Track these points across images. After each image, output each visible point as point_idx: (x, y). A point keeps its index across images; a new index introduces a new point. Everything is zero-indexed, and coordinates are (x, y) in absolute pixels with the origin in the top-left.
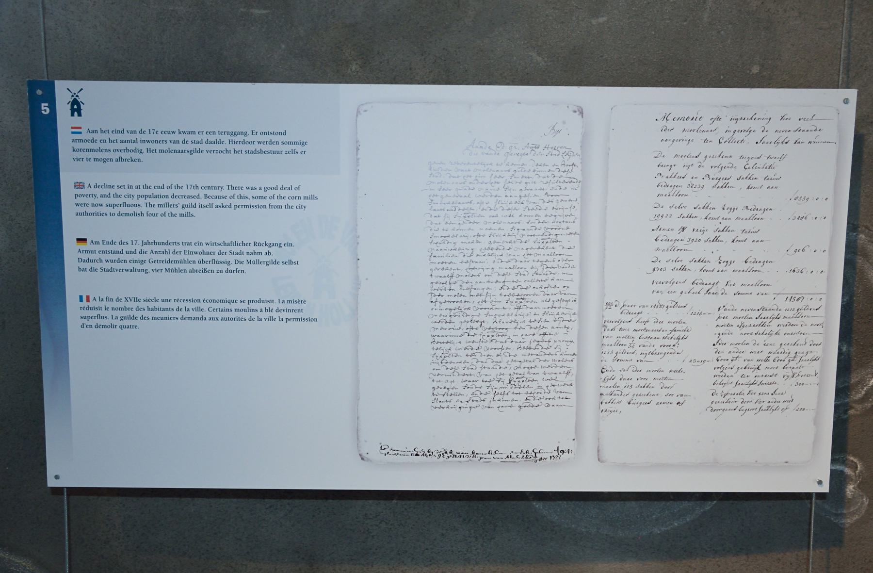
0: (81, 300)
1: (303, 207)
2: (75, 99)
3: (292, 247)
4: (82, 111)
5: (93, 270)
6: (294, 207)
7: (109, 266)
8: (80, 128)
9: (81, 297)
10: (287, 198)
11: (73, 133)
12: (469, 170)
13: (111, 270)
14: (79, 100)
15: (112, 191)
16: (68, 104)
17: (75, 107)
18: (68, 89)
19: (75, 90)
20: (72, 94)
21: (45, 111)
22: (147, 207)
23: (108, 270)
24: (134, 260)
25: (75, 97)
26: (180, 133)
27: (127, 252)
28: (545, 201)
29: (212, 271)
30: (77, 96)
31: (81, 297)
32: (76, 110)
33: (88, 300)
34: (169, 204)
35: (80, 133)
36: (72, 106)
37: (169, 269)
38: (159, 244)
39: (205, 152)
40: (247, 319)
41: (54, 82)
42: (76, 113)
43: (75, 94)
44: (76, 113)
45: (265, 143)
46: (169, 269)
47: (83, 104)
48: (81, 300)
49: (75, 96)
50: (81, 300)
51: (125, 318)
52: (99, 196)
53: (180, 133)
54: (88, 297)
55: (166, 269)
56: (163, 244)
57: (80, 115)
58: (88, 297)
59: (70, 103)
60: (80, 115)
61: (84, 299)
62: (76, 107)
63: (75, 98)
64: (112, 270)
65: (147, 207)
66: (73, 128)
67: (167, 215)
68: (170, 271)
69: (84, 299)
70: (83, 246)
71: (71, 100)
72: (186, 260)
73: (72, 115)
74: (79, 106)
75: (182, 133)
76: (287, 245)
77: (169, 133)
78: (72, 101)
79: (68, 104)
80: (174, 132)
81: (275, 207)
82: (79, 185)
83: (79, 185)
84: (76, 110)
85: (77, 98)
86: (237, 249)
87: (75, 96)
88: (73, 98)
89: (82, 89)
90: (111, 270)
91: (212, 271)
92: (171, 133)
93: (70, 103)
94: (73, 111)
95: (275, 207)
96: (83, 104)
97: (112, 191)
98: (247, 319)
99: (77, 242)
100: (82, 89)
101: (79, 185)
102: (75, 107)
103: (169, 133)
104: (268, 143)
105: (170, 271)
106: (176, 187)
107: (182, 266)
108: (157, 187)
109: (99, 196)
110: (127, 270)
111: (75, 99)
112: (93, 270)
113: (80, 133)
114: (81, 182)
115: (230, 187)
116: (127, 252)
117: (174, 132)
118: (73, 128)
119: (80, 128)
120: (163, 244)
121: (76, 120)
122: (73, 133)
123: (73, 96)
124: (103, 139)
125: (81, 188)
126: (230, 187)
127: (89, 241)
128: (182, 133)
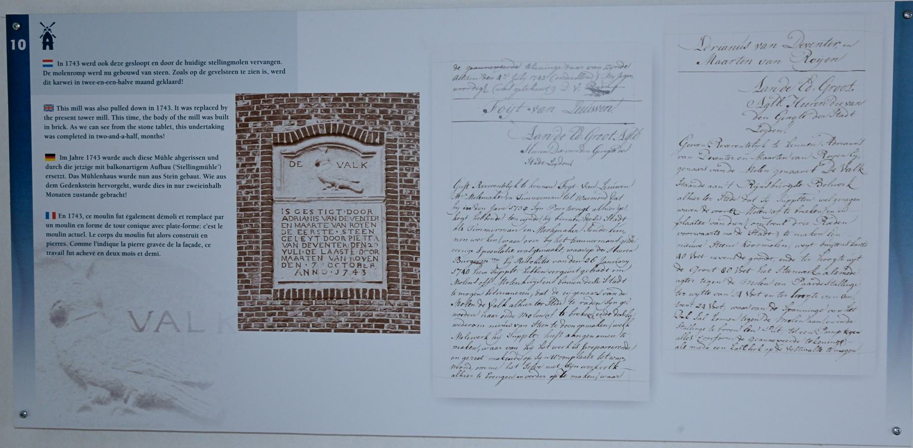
0: (47, 217)
2: (47, 33)
3: (108, 120)
8: (51, 61)
9: (47, 214)
11: (44, 66)
12: (517, 111)
14: (51, 34)
16: (41, 37)
17: (47, 40)
18: (41, 23)
20: (44, 28)
22: (58, 110)
24: (91, 135)
25: (47, 31)
27: (176, 177)
28: (583, 143)
30: (50, 30)
31: (47, 214)
32: (47, 43)
33: (54, 217)
34: (122, 107)
35: (51, 66)
37: (159, 156)
42: (48, 47)
43: (47, 28)
44: (48, 47)
46: (159, 156)
47: (55, 37)
48: (47, 217)
49: (47, 29)
51: (134, 245)
54: (54, 214)
55: (156, 156)
57: (51, 48)
58: (54, 214)
61: (51, 216)
65: (58, 110)
66: (44, 61)
67: (176, 117)
68: (160, 158)
69: (51, 216)
70: (51, 162)
71: (44, 34)
72: (211, 165)
73: (44, 48)
76: (90, 186)
79: (41, 37)
85: (49, 32)
88: (45, 32)
89: (54, 23)
96: (55, 37)
100: (54, 23)
101: (48, 108)
102: (47, 40)
105: (160, 158)
111: (47, 33)
113: (51, 66)
115: (60, 108)
116: (176, 177)
118: (44, 61)
119: (51, 61)
121: (48, 52)
122: (44, 66)
123: (45, 30)
127: (57, 157)
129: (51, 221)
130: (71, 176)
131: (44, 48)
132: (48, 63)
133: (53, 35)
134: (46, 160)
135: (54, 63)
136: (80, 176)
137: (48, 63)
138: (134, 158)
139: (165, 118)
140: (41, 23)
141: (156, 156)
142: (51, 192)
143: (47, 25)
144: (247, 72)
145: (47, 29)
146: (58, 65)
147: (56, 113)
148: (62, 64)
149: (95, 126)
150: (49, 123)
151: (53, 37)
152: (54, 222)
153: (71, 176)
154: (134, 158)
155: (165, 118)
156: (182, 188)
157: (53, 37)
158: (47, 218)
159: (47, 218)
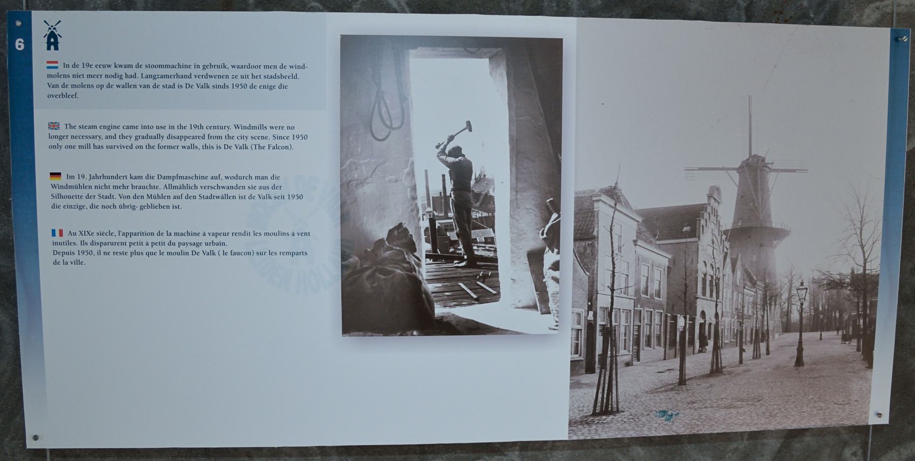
0: (54, 234)
1: (245, 137)
4: (59, 44)
5: (94, 207)
6: (236, 138)
7: (207, 193)
8: (56, 62)
9: (54, 231)
10: (121, 127)
11: (48, 67)
13: (210, 197)
14: (56, 33)
15: (118, 132)
16: (45, 37)
17: (52, 40)
19: (52, 23)
20: (49, 27)
21: (20, 42)
23: (207, 198)
25: (52, 30)
26: (116, 67)
29: (234, 197)
30: (55, 29)
31: (54, 231)
32: (52, 43)
35: (57, 67)
36: (49, 39)
37: (151, 195)
38: (108, 178)
39: (115, 87)
40: (89, 243)
41: (30, 13)
42: (52, 47)
43: (52, 26)
44: (52, 47)
45: (201, 77)
46: (151, 195)
47: (61, 37)
48: (54, 234)
50: (54, 234)
52: (103, 137)
53: (116, 67)
54: (61, 231)
55: (148, 195)
56: (112, 177)
57: (56, 48)
58: (61, 231)
59: (47, 36)
60: (56, 48)
61: (57, 233)
62: (53, 40)
63: (51, 31)
64: (211, 197)
66: (48, 62)
69: (57, 233)
70: (56, 181)
71: (48, 33)
73: (49, 49)
74: (56, 39)
75: (118, 66)
76: (66, 207)
77: (104, 66)
78: (49, 34)
79: (45, 37)
80: (109, 66)
81: (215, 138)
82: (54, 126)
83: (54, 126)
84: (52, 43)
85: (54, 31)
86: (102, 182)
87: (52, 28)
88: (50, 31)
89: (60, 22)
90: (210, 197)
91: (234, 197)
92: (106, 66)
93: (47, 36)
94: (49, 44)
95: (215, 138)
96: (61, 37)
97: (118, 132)
98: (89, 243)
99: (51, 177)
101: (54, 126)
102: (52, 40)
103: (104, 66)
104: (203, 77)
106: (179, 128)
107: (231, 192)
108: (212, 128)
109: (103, 137)
110: (218, 197)
112: (94, 207)
113: (57, 67)
114: (56, 123)
115: (68, 126)
117: (109, 66)
118: (48, 62)
119: (56, 62)
120: (112, 177)
121: (52, 54)
122: (48, 67)
123: (50, 29)
124: (262, 85)
125: (56, 129)
126: (68, 126)
128: (118, 66)
129: (57, 238)
130: (160, 177)
131: (49, 49)
132: (52, 65)
133: (58, 35)
134: (51, 179)
135: (60, 65)
136: (146, 197)
137: (52, 65)
138: (250, 177)
139: (161, 137)
140: (45, 21)
141: (148, 195)
142: (78, 72)
143: (52, 23)
144: (62, 207)
145: (52, 28)
146: (64, 67)
147: (62, 181)
148: (68, 66)
149: (129, 125)
150: (56, 191)
151: (58, 36)
152: (61, 239)
153: (160, 177)
154: (250, 177)
155: (161, 137)
156: (227, 236)
157: (58, 36)
158: (55, 230)
159: (55, 230)
